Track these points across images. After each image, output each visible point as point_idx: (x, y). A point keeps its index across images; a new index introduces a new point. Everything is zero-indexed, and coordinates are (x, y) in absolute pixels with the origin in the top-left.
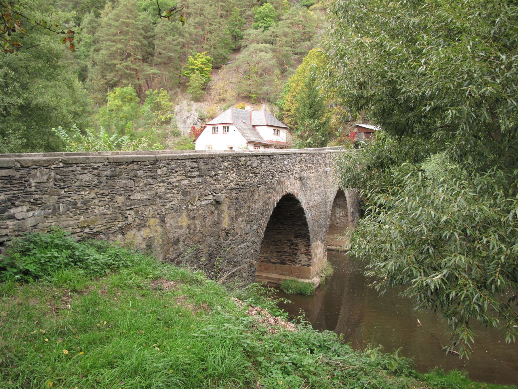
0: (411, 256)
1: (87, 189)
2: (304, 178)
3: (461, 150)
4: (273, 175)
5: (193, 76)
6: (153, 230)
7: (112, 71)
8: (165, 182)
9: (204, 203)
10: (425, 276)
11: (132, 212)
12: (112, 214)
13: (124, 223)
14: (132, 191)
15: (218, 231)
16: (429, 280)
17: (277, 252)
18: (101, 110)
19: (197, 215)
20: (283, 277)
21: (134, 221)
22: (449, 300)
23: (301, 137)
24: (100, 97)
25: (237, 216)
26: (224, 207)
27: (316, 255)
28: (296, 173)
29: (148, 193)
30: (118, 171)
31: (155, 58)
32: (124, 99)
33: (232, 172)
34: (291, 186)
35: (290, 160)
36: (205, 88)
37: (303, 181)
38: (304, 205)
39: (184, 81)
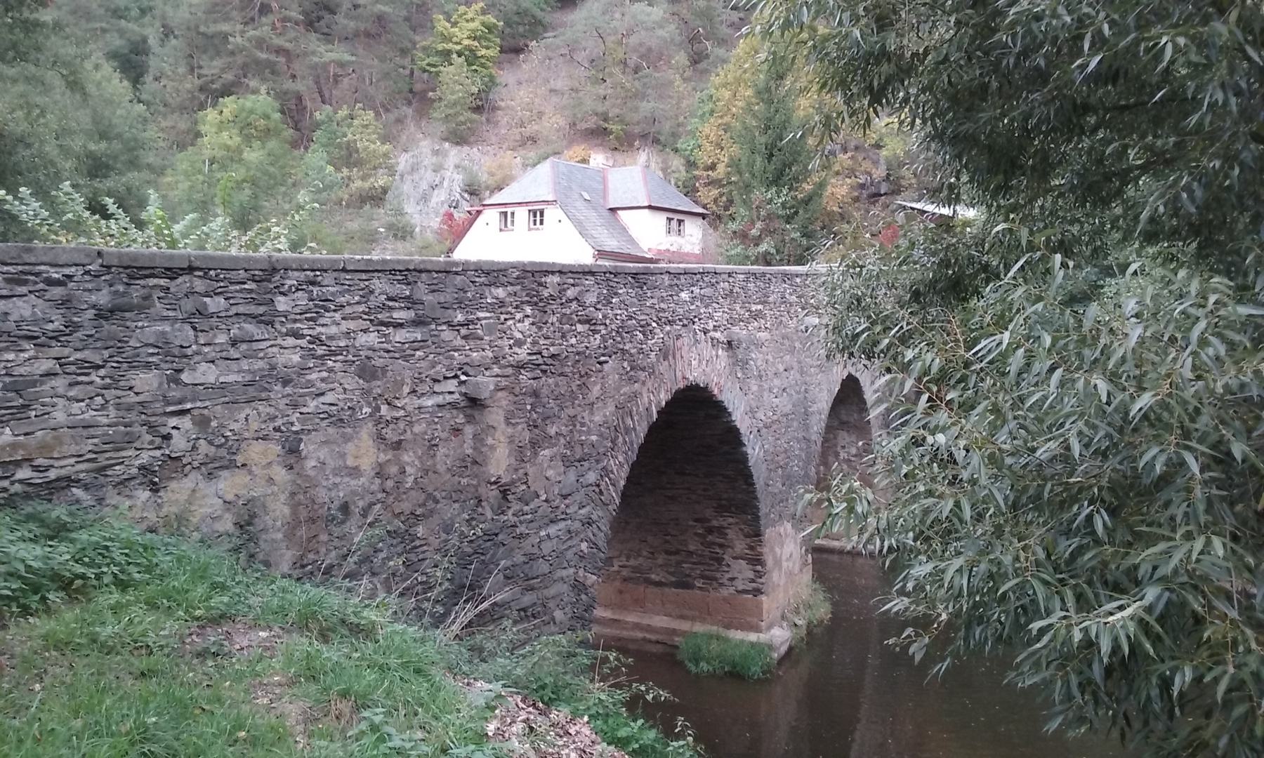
0: (1031, 542)
1: (26, 345)
2: (740, 342)
3: (1207, 187)
4: (645, 329)
5: (447, 72)
6: (262, 476)
7: (218, 54)
8: (303, 336)
9: (429, 402)
10: (1078, 611)
11: (186, 423)
12: (116, 425)
13: (158, 453)
14: (186, 356)
15: (476, 487)
16: (1092, 624)
17: (668, 553)
18: (182, 161)
19: (408, 435)
20: (685, 626)
21: (194, 448)
22: (1170, 696)
23: (743, 236)
24: (183, 125)
25: (535, 445)
26: (495, 416)
27: (778, 562)
28: (715, 328)
29: (245, 364)
30: (136, 294)
31: (340, 19)
32: (248, 129)
33: (518, 316)
34: (701, 364)
35: (696, 290)
36: (482, 105)
37: (738, 351)
38: (740, 418)
39: (424, 86)
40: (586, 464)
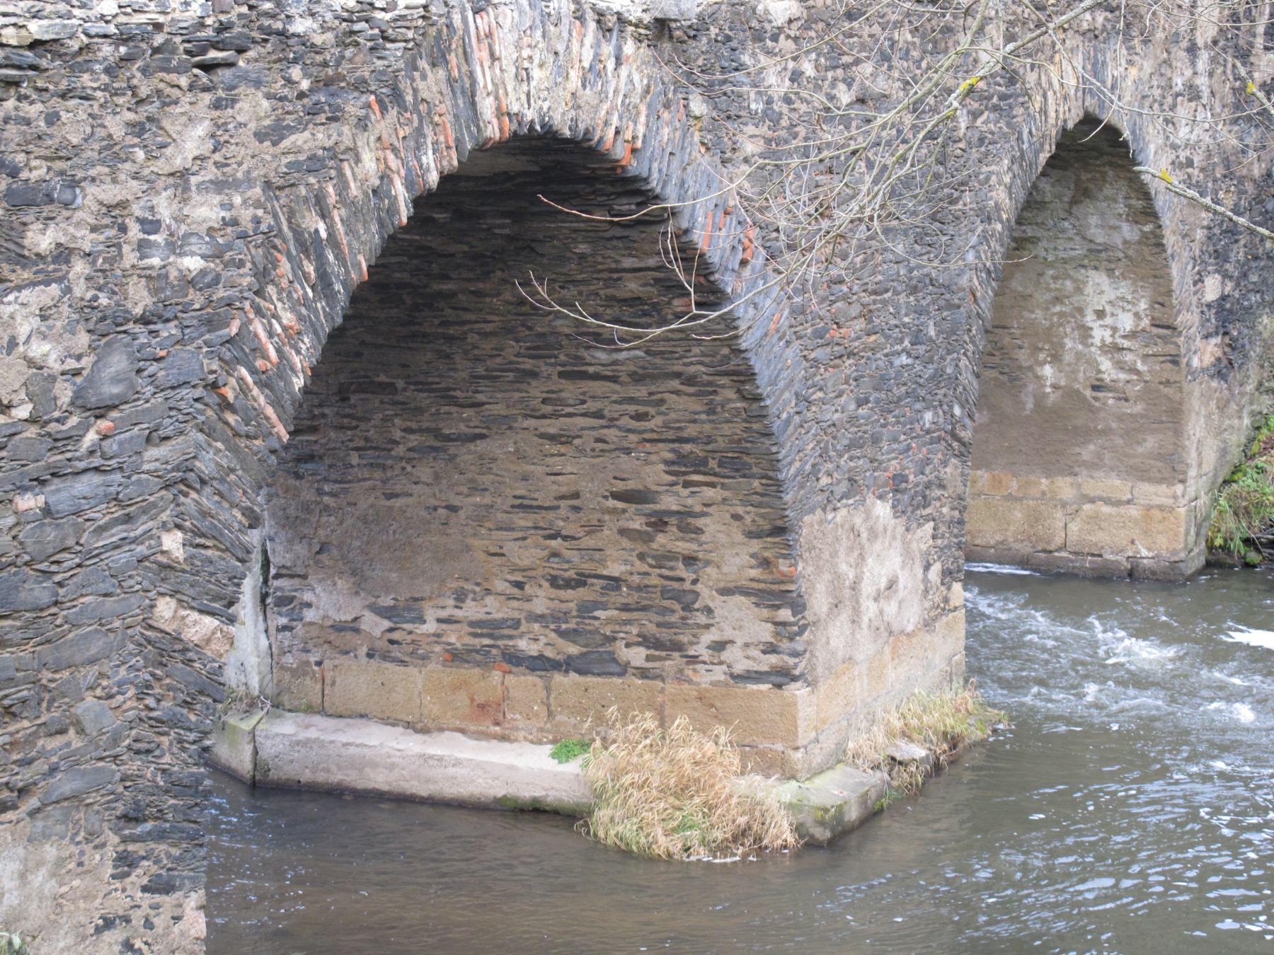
27: (846, 597)
40: (171, 329)
